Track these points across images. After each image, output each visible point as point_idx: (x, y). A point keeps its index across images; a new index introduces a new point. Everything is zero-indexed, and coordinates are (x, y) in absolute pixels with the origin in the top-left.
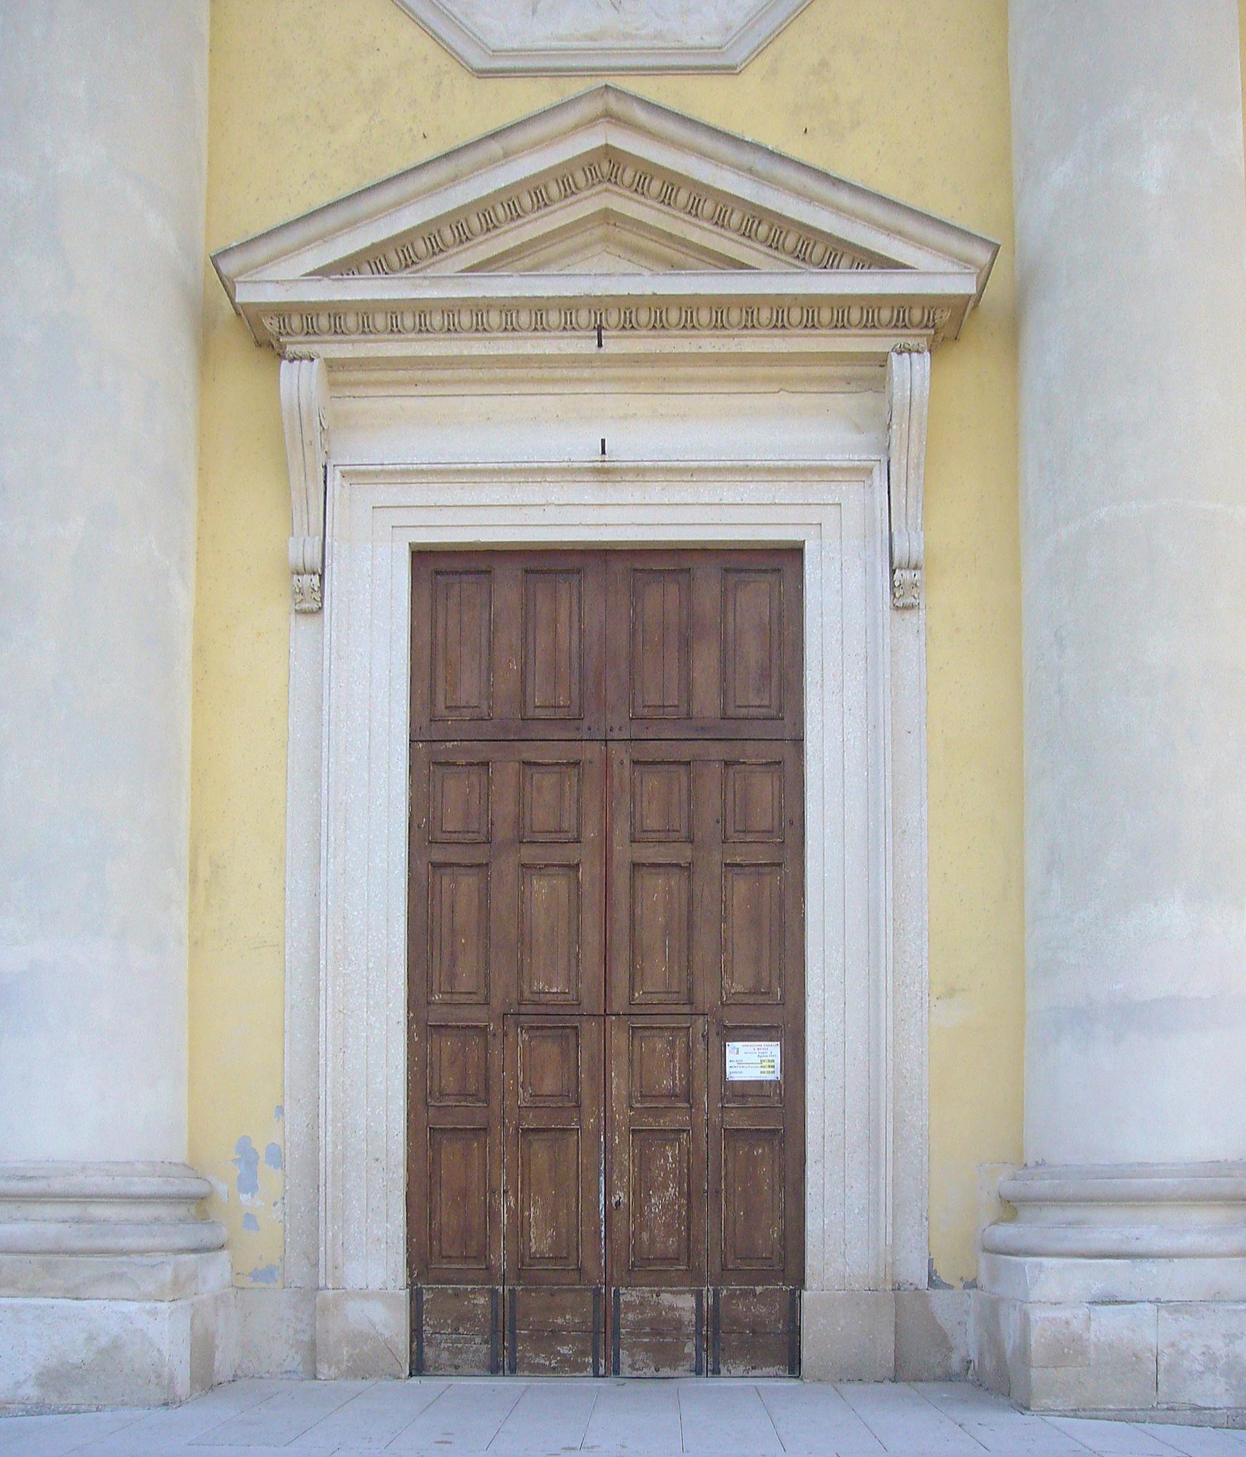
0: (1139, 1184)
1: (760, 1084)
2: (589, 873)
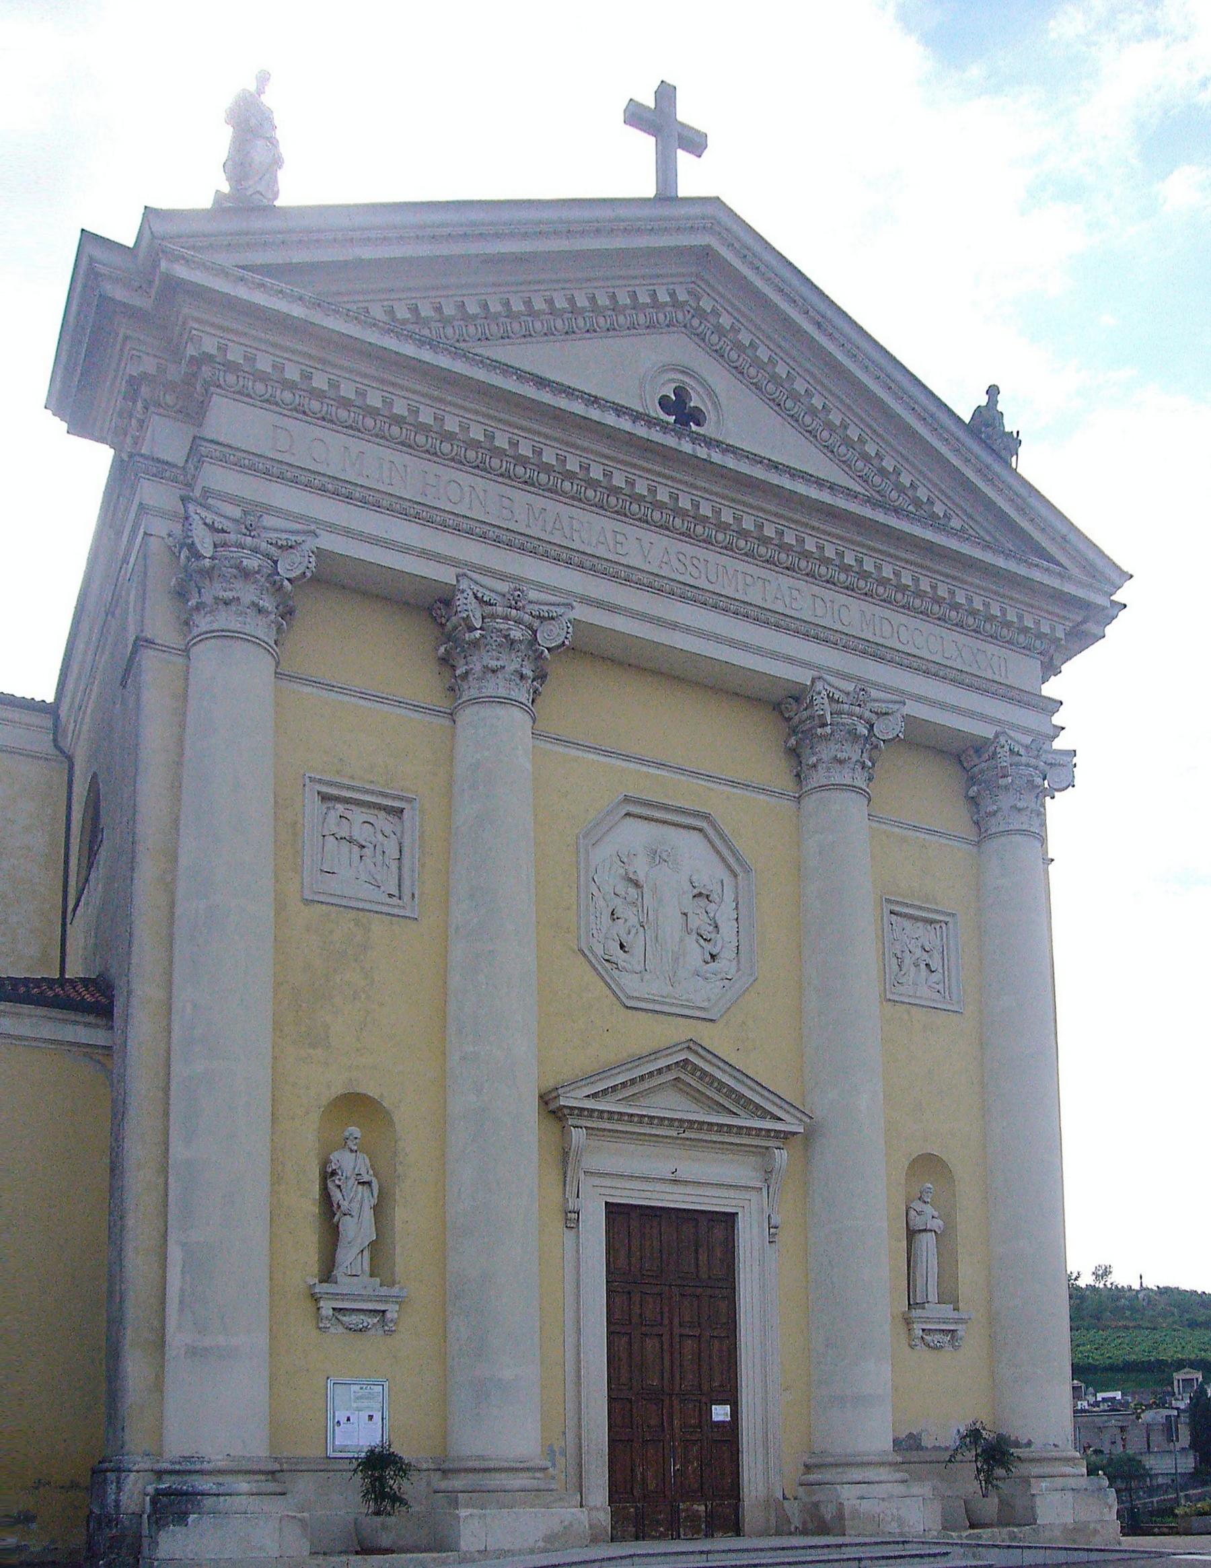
0: (865, 1459)
1: (724, 1422)
2: (666, 1338)
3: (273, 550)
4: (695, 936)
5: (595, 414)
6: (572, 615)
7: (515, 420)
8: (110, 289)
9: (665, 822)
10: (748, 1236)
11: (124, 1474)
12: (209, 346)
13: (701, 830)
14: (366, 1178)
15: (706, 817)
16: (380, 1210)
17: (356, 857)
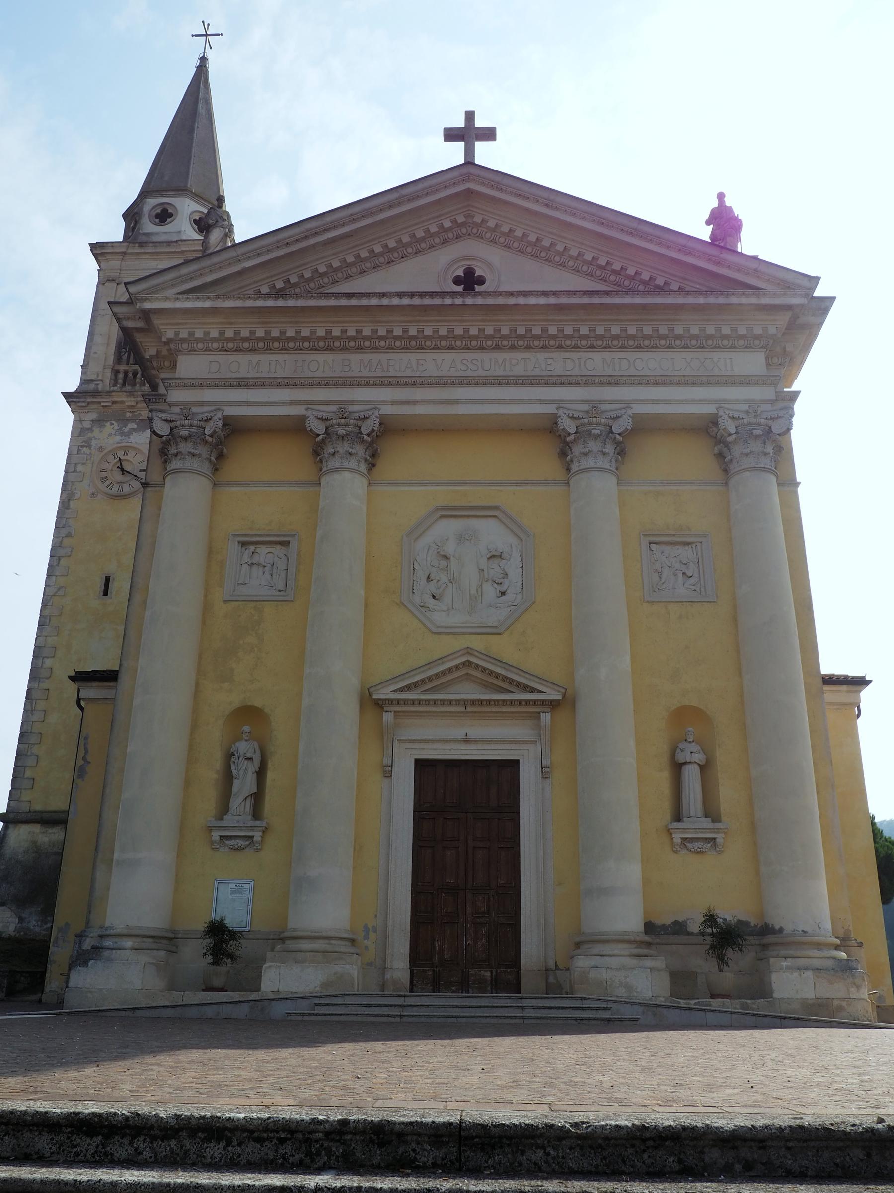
3: (202, 423)
4: (490, 582)
5: (385, 302)
6: (630, 412)
7: (347, 319)
8: (130, 324)
9: (468, 517)
10: (528, 776)
11: (84, 939)
12: (170, 334)
13: (494, 517)
14: (249, 755)
15: (497, 508)
16: (261, 774)
17: (261, 573)
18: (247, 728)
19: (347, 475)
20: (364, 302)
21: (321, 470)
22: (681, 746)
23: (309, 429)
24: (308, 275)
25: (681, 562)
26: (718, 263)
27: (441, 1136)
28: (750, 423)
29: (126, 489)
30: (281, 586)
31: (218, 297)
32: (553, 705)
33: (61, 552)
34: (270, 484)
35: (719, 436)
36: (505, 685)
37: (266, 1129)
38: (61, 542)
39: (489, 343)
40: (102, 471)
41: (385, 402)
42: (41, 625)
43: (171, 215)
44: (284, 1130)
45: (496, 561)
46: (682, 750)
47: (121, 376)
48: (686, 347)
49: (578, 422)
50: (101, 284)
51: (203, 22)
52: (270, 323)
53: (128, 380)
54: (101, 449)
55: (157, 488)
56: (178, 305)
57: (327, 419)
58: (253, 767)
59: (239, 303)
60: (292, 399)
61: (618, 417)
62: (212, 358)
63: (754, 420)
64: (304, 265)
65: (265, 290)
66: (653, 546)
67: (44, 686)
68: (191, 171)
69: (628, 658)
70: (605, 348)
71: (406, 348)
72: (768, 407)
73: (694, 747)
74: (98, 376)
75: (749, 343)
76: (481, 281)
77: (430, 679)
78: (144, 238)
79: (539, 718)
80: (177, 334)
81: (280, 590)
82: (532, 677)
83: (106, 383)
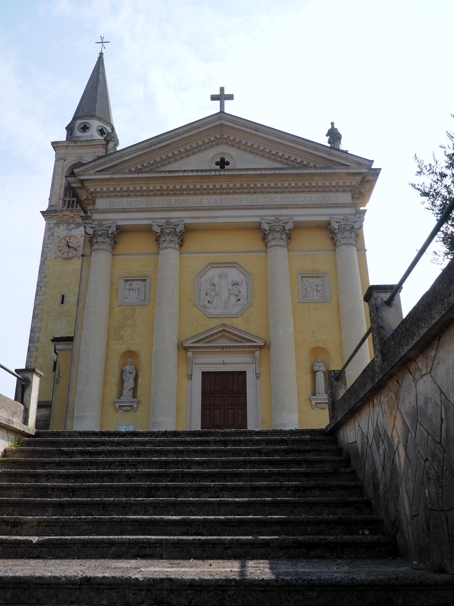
3: (107, 228)
4: (233, 295)
5: (186, 174)
9: (224, 267)
12: (92, 189)
13: (235, 267)
14: (131, 371)
16: (136, 379)
18: (129, 360)
19: (170, 250)
20: (177, 174)
21: (159, 248)
22: (316, 364)
23: (153, 230)
24: (152, 162)
25: (316, 285)
26: (330, 155)
27: (189, 434)
28: (344, 224)
29: (70, 255)
30: (143, 299)
31: (113, 174)
32: (260, 348)
33: (42, 284)
34: (137, 254)
35: (331, 230)
36: (240, 340)
37: (148, 433)
38: (41, 280)
39: (231, 191)
40: (59, 247)
41: (186, 218)
42: (34, 318)
43: (88, 128)
44: (152, 433)
45: (235, 286)
46: (316, 366)
47: (67, 203)
48: (317, 191)
49: (270, 225)
50: (57, 160)
51: (101, 37)
52: (135, 184)
53: (70, 205)
54: (58, 237)
55: (88, 257)
56: (96, 177)
57: (161, 226)
58: (132, 376)
59: (122, 176)
60: (146, 217)
61: (287, 223)
62: (111, 200)
63: (346, 223)
64: (150, 158)
65: (133, 169)
66: (303, 278)
67: (36, 345)
68: (97, 107)
69: (292, 327)
70: (282, 192)
71: (195, 194)
72: (353, 217)
73: (321, 364)
74: (56, 203)
75: (344, 189)
76: (228, 163)
77: (208, 337)
78: (76, 139)
79: (254, 353)
80: (95, 189)
81: (142, 301)
82: (251, 336)
83: (60, 207)
